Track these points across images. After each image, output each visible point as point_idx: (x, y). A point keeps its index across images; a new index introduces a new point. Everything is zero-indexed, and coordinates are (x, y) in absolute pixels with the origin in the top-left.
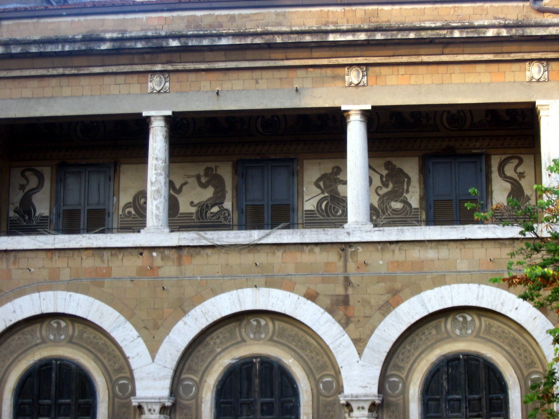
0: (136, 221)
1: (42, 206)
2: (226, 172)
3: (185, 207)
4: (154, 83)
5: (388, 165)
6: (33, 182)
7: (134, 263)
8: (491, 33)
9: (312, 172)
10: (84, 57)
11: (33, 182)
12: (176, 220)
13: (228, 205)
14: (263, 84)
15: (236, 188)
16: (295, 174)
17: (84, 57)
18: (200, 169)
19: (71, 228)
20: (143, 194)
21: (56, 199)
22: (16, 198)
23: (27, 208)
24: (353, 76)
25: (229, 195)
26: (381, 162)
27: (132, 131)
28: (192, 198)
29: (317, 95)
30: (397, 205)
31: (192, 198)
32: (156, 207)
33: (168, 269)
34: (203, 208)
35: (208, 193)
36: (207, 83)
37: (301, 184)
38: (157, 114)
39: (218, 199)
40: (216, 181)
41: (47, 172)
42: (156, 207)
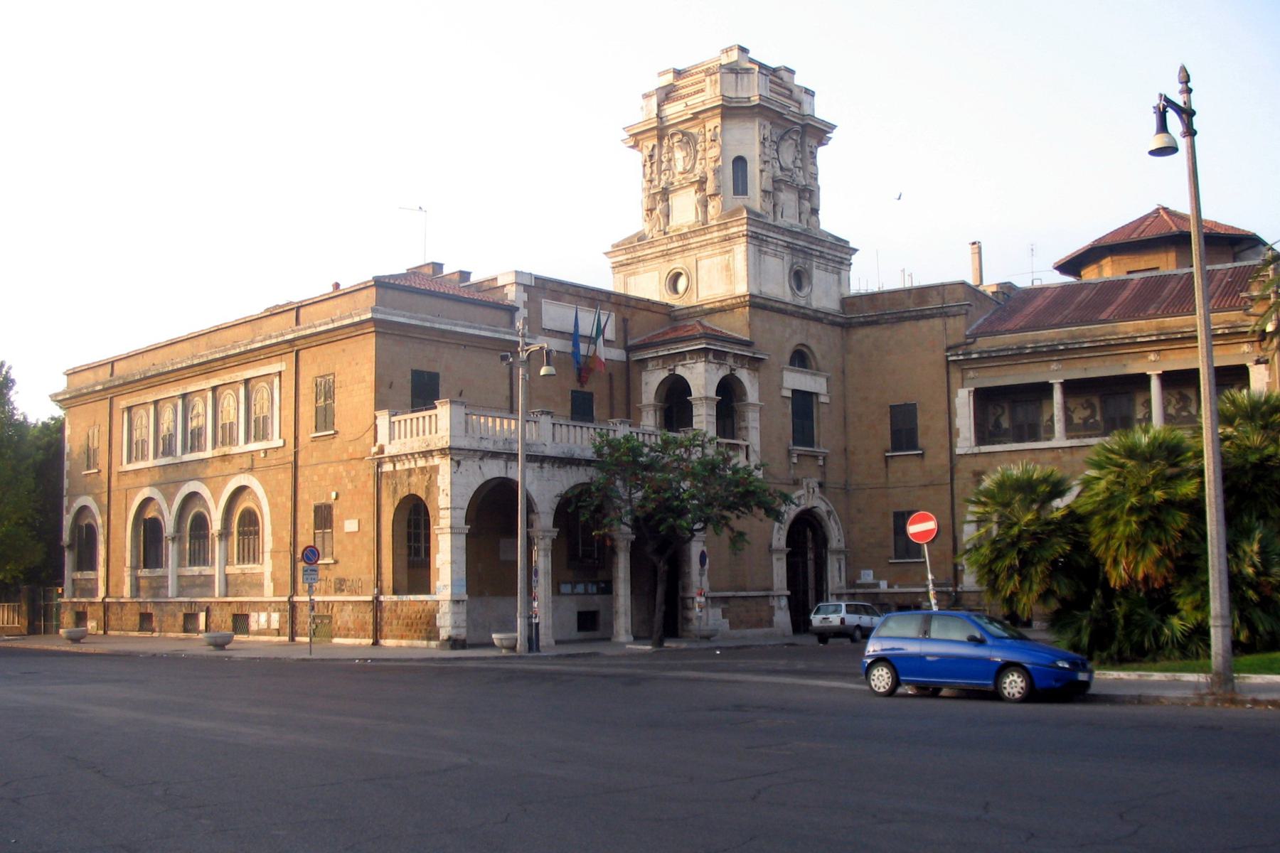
0: (1050, 433)
1: (1005, 424)
2: (1096, 401)
3: (1077, 419)
4: (1054, 366)
5: (1180, 393)
6: (1000, 411)
7: (1049, 456)
8: (1219, 332)
9: (1140, 399)
10: (1017, 356)
11: (1000, 411)
12: (1071, 429)
13: (1098, 418)
14: (1107, 363)
15: (1102, 408)
16: (1132, 401)
17: (1017, 356)
18: (1082, 400)
19: (1020, 439)
20: (1052, 417)
21: (1012, 419)
22: (992, 420)
23: (997, 424)
24: (1152, 357)
25: (1098, 409)
26: (1174, 392)
27: (1046, 389)
28: (1079, 416)
29: (1134, 368)
30: (1185, 414)
31: (1079, 416)
32: (1059, 427)
33: (1066, 458)
34: (1085, 420)
35: (1087, 413)
36: (1079, 364)
37: (1134, 406)
38: (1056, 382)
39: (1093, 416)
40: (1091, 406)
41: (1006, 406)
42: (1059, 427)
